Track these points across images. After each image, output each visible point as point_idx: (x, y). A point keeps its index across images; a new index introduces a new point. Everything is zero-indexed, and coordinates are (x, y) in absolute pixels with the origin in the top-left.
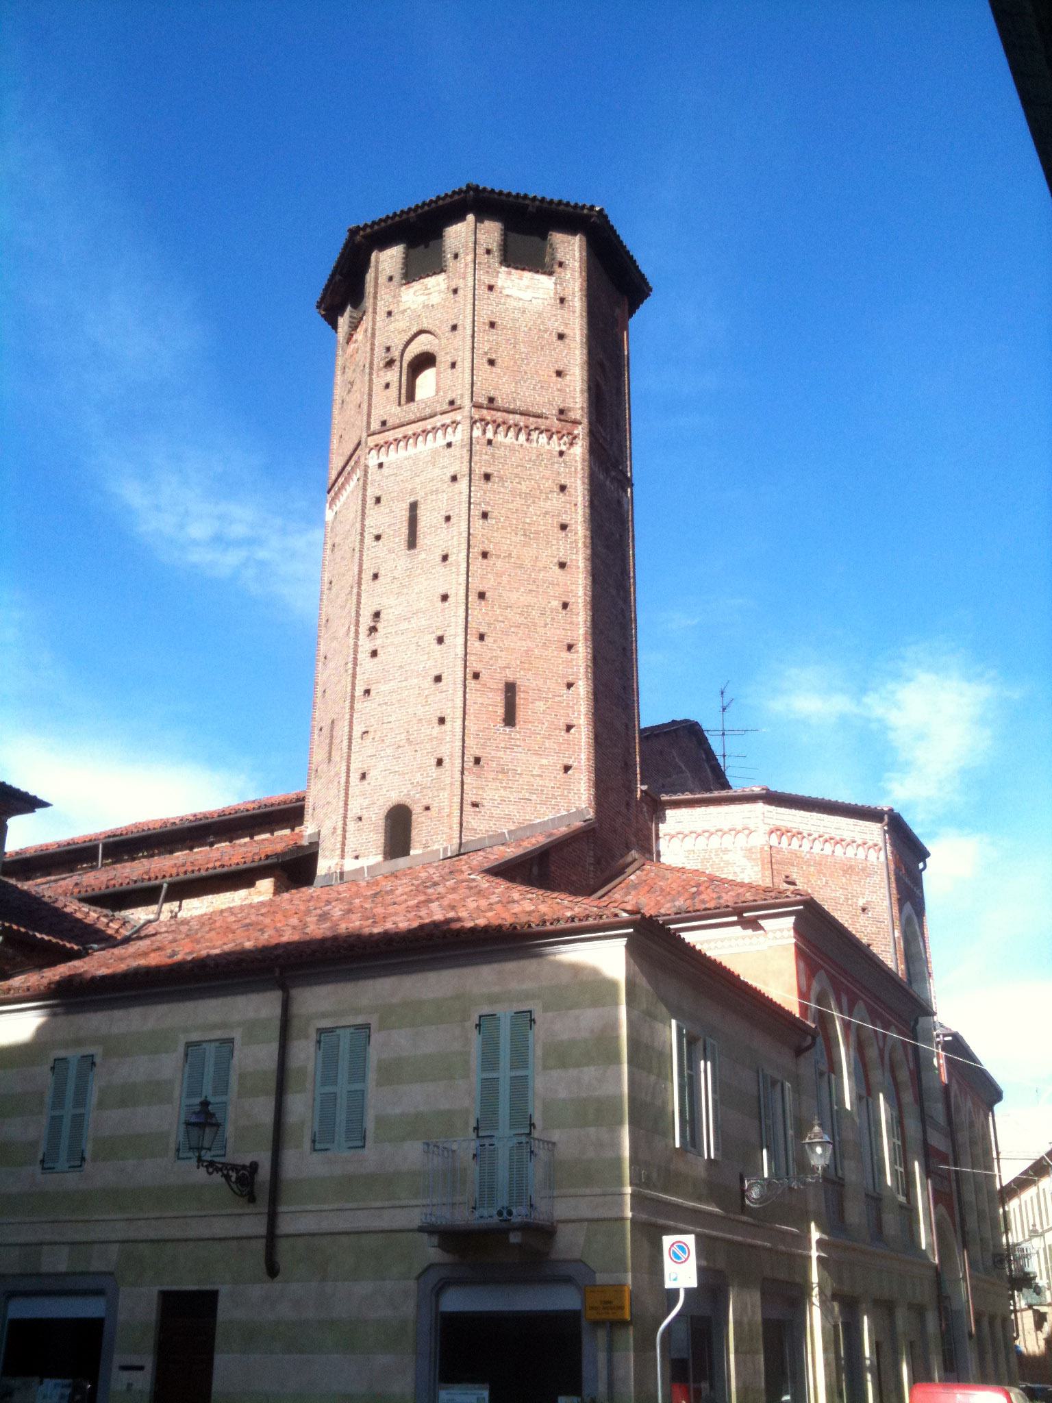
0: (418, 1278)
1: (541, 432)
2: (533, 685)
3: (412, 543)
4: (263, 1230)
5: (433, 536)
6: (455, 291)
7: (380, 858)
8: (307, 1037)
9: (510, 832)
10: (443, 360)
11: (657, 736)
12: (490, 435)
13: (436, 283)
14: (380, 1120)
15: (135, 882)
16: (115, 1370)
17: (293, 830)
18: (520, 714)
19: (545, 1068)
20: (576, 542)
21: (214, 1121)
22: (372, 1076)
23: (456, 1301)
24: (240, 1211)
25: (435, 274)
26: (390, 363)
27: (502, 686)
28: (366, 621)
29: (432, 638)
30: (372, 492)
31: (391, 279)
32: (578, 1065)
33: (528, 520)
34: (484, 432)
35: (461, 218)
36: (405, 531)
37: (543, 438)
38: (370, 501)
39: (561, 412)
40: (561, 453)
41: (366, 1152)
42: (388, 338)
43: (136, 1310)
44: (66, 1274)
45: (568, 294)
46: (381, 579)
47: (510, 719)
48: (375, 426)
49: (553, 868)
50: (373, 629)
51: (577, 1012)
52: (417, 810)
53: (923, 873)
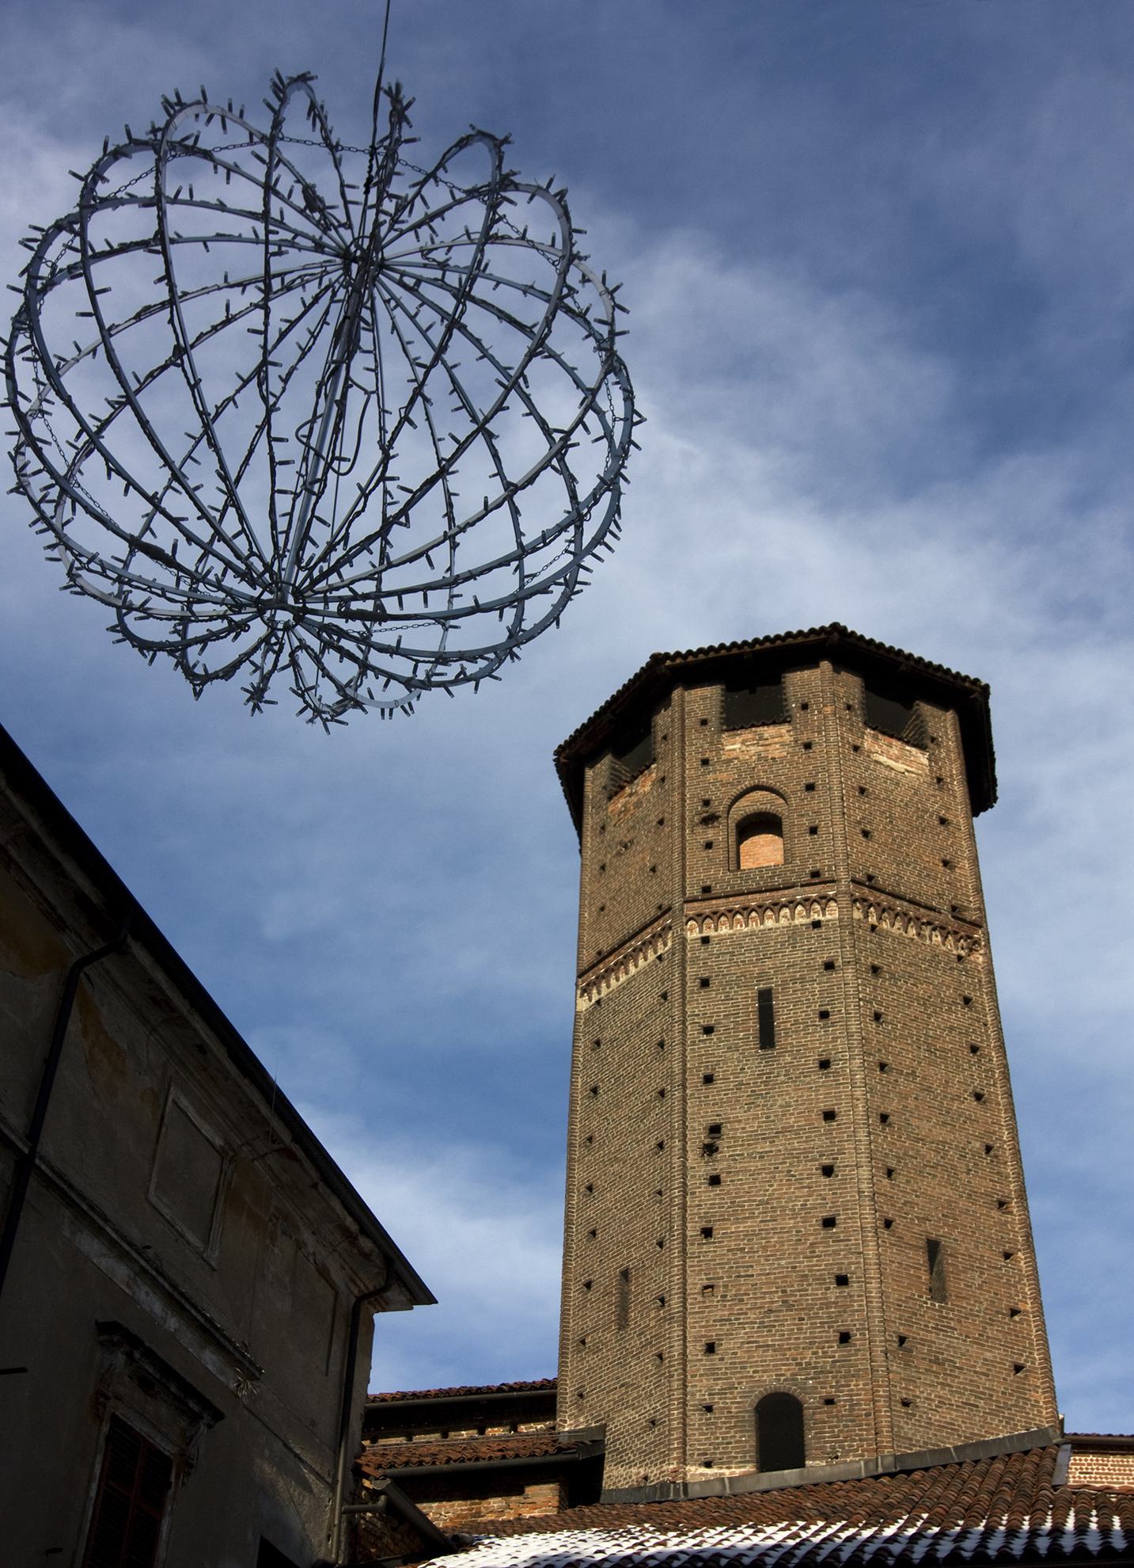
1: (934, 929)
3: (767, 1038)
7: (750, 1468)
9: (956, 1448)
12: (873, 920)
13: (776, 739)
17: (445, 1435)
20: (991, 1070)
25: (774, 723)
26: (709, 820)
27: (922, 1243)
34: (866, 916)
35: (813, 664)
36: (754, 1025)
37: (937, 938)
39: (954, 908)
45: (945, 773)
46: (719, 1084)
48: (693, 890)
50: (710, 1149)
52: (811, 1401)
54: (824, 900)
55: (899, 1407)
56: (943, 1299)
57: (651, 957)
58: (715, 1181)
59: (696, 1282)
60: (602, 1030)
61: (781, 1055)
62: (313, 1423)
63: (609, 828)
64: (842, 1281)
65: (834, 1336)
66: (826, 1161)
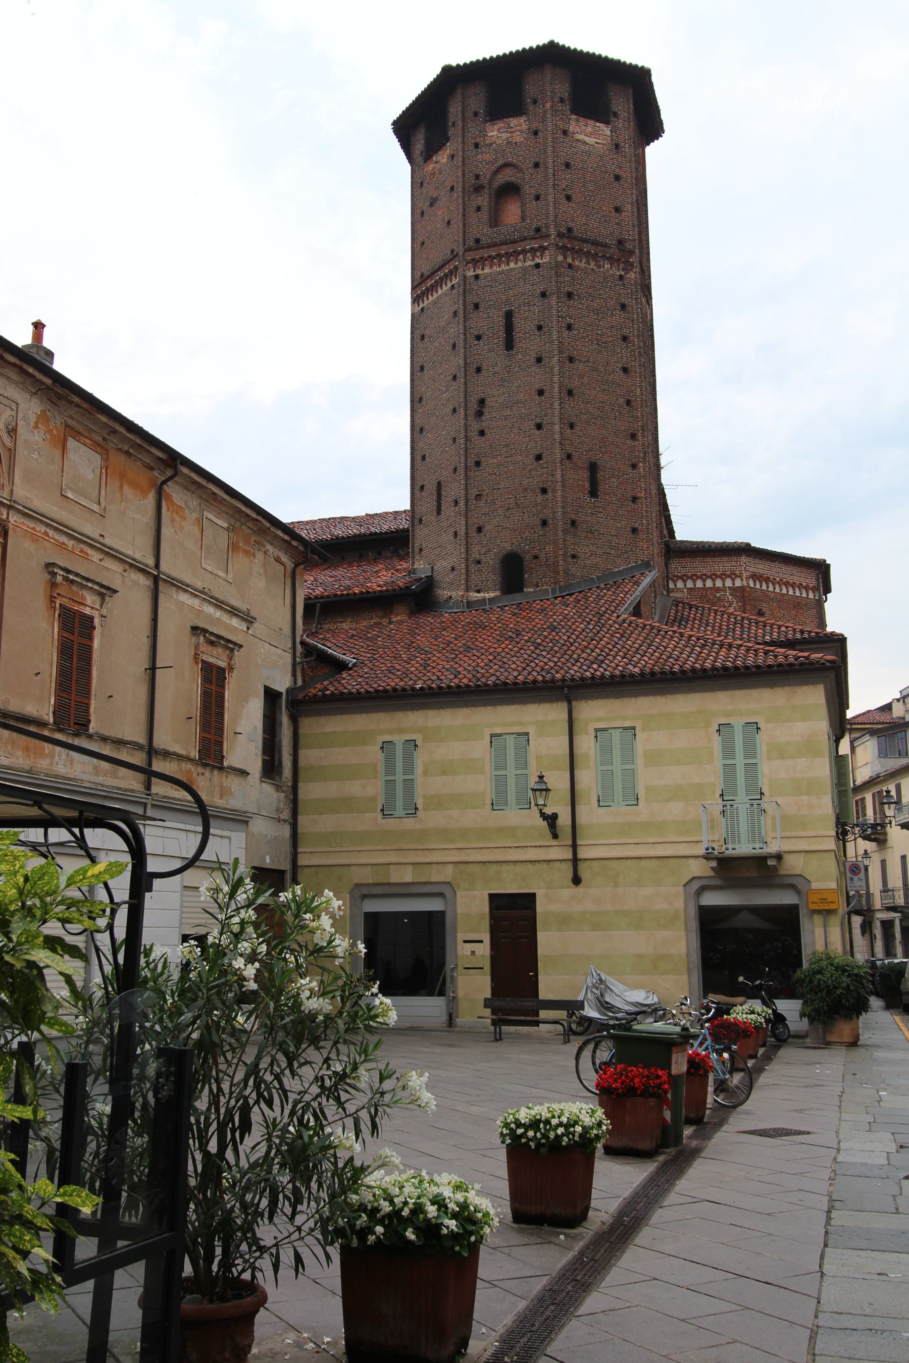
0: (684, 886)
3: (509, 344)
5: (529, 343)
6: (536, 133)
7: (498, 593)
8: (587, 734)
10: (528, 191)
12: (569, 260)
13: (519, 124)
18: (602, 487)
19: (769, 759)
22: (640, 761)
23: (712, 899)
26: (478, 189)
27: (586, 465)
28: (473, 406)
29: (532, 424)
33: (600, 332)
34: (565, 258)
36: (502, 334)
38: (470, 307)
40: (621, 277)
41: (640, 807)
46: (484, 373)
47: (594, 493)
51: (790, 724)
52: (528, 557)
53: (825, 604)
54: (543, 249)
55: (570, 559)
57: (449, 285)
58: (482, 433)
59: (473, 492)
60: (425, 328)
61: (517, 354)
62: (280, 629)
63: (425, 185)
64: (544, 491)
65: (538, 522)
66: (538, 421)
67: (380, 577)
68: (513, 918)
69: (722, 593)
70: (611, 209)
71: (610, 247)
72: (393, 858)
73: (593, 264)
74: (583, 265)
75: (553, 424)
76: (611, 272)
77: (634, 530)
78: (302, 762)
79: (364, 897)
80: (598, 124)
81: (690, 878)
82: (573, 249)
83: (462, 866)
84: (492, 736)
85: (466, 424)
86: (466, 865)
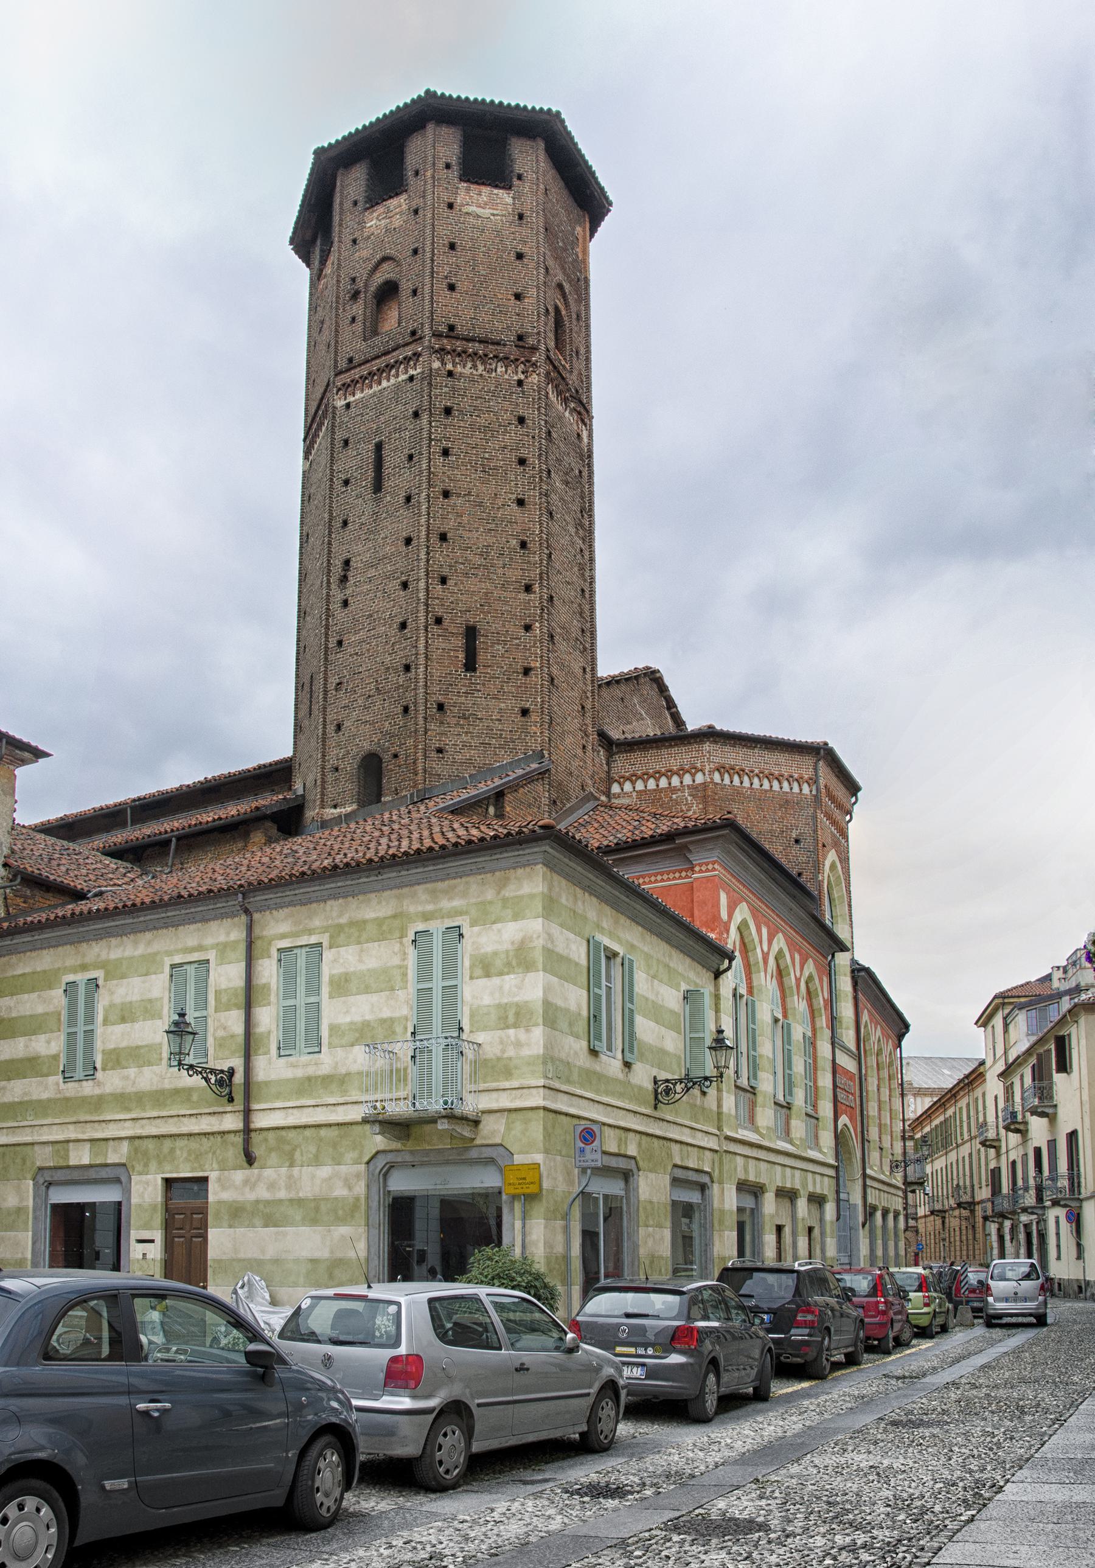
0: (368, 1163)
2: (493, 629)
4: (240, 1126)
5: (398, 481)
6: (416, 212)
7: (355, 806)
10: (406, 287)
11: (618, 682)
12: (449, 367)
13: (398, 204)
14: (333, 1028)
15: (149, 836)
16: (133, 1242)
18: (482, 657)
19: (471, 978)
21: (190, 1030)
22: (325, 990)
24: (221, 1110)
28: (337, 570)
30: (340, 435)
31: (355, 203)
32: (501, 974)
33: (487, 455)
34: (443, 363)
38: (339, 444)
39: (520, 338)
40: (520, 383)
41: (321, 1056)
42: (354, 268)
43: (146, 1192)
44: (91, 1166)
46: (350, 526)
47: (470, 665)
48: (343, 364)
49: (508, 809)
51: (499, 926)
52: (386, 757)
55: (434, 754)
56: (474, 670)
59: (333, 681)
65: (400, 709)
66: (404, 578)
67: (268, 801)
68: (186, 1210)
69: (680, 794)
70: (509, 297)
71: (505, 345)
72: (71, 1133)
73: (481, 368)
74: (467, 370)
75: (418, 580)
76: (506, 377)
77: (525, 712)
78: (561, 1095)
79: (49, 1184)
80: (496, 191)
81: (374, 1152)
82: (454, 351)
83: (137, 1142)
84: (173, 966)
85: (328, 595)
86: (140, 1141)
